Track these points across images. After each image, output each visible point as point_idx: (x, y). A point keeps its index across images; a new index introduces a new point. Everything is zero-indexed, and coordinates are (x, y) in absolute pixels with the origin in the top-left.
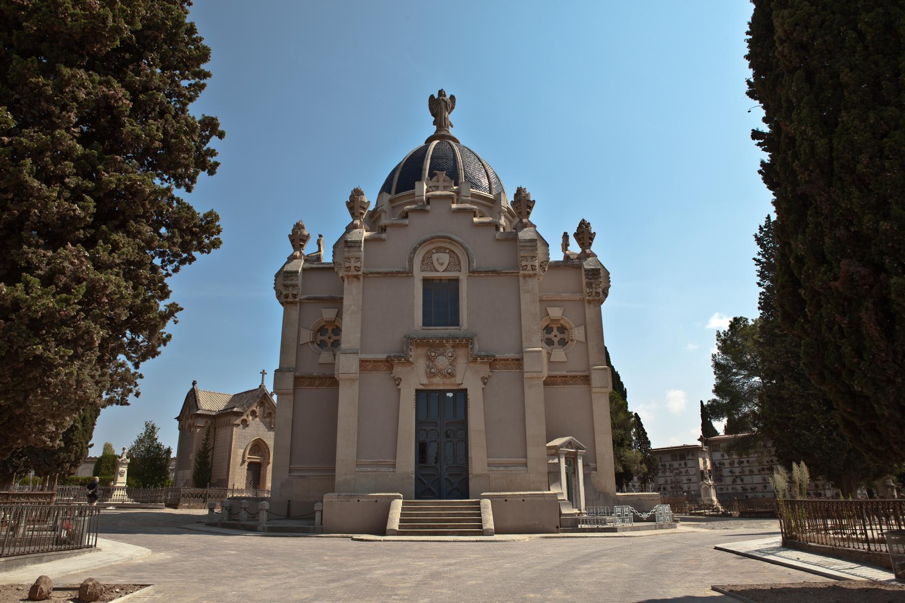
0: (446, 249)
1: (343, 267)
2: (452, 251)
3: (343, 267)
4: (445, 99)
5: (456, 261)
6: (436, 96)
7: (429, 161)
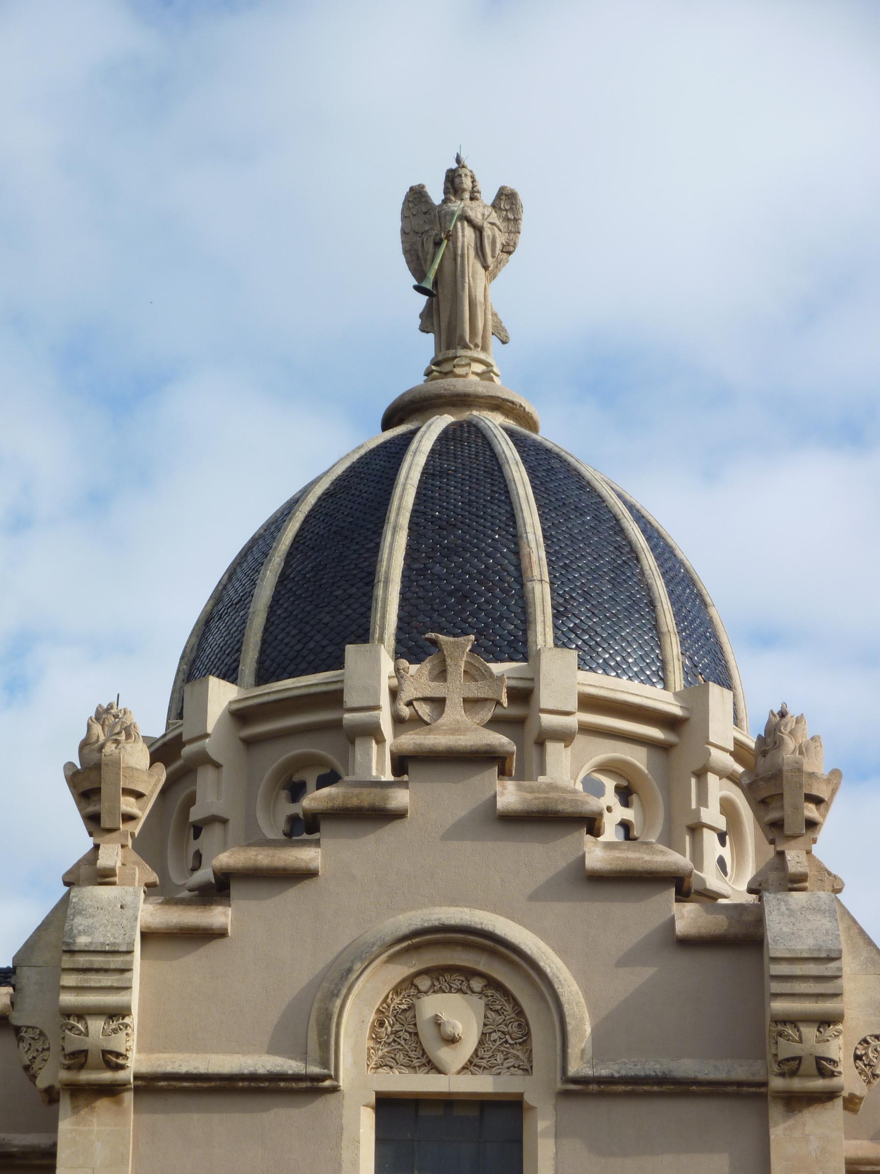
0: (470, 973)
1: (55, 1048)
2: (492, 983)
3: (55, 1048)
4: (477, 212)
5: (513, 1028)
6: (436, 195)
7: (401, 541)
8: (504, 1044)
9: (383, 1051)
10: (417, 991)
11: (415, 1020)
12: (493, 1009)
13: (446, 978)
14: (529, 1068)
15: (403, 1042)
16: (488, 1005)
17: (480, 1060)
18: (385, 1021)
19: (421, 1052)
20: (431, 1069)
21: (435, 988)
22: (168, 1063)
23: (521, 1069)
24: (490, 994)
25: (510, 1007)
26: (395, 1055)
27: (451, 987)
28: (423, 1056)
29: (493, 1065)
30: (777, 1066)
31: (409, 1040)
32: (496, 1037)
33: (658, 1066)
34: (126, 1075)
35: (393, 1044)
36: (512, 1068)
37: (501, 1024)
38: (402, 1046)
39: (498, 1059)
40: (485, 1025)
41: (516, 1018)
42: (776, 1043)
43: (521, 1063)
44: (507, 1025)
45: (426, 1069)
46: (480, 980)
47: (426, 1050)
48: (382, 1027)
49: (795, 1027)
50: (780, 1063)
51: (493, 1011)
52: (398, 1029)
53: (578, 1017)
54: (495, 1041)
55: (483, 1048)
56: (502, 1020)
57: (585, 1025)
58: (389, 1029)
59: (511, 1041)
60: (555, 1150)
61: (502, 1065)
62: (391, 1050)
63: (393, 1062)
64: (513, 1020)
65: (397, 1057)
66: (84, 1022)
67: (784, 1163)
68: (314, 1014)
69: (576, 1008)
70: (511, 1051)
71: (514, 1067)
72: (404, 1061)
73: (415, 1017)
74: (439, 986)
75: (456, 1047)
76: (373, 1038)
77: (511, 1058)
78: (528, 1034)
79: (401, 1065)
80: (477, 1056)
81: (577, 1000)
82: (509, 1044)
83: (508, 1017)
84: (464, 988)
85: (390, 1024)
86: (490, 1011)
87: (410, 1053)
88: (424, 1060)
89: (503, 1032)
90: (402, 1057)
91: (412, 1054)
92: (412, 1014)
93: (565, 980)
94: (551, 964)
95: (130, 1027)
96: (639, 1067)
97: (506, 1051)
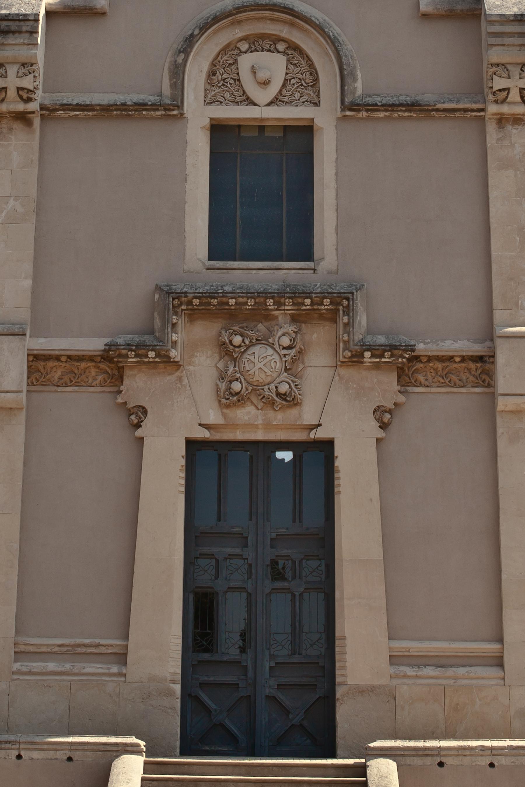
8: (300, 87)
9: (215, 92)
10: (239, 52)
11: (238, 71)
12: (293, 63)
13: (260, 42)
14: (317, 102)
15: (229, 86)
16: (289, 60)
17: (283, 97)
18: (217, 72)
19: (242, 92)
20: (249, 103)
21: (252, 49)
22: (64, 99)
23: (312, 103)
24: (290, 53)
25: (304, 62)
26: (224, 94)
27: (263, 49)
28: (243, 95)
29: (292, 101)
30: (492, 95)
31: (234, 84)
32: (295, 82)
33: (408, 99)
34: (34, 106)
35: (222, 87)
36: (306, 102)
37: (298, 73)
38: (229, 88)
39: (296, 97)
40: (287, 74)
41: (309, 69)
42: (492, 79)
43: (312, 99)
44: (302, 74)
45: (246, 103)
46: (283, 44)
47: (246, 90)
48: (215, 76)
49: (505, 68)
50: (494, 94)
51: (292, 65)
52: (226, 77)
53: (352, 66)
54: (294, 84)
55: (286, 89)
56: (299, 70)
57: (357, 72)
58: (220, 77)
59: (304, 84)
60: (336, 156)
61: (299, 101)
62: (221, 91)
63: (222, 99)
64: (306, 70)
65: (225, 95)
66: (4, 68)
67: (497, 163)
68: (167, 66)
69: (350, 60)
70: (305, 91)
71: (308, 102)
72: (230, 98)
73: (238, 69)
74: (254, 48)
75: (267, 88)
76: (209, 83)
77: (305, 96)
78: (316, 80)
79: (228, 101)
80: (281, 95)
81: (352, 55)
82: (304, 86)
83: (303, 69)
84: (272, 49)
85: (220, 74)
86: (290, 65)
87: (234, 92)
88: (244, 98)
89: (299, 79)
90: (229, 95)
91: (235, 93)
92: (235, 67)
93: (343, 42)
94: (333, 30)
95: (37, 72)
96: (395, 99)
97: (301, 91)
